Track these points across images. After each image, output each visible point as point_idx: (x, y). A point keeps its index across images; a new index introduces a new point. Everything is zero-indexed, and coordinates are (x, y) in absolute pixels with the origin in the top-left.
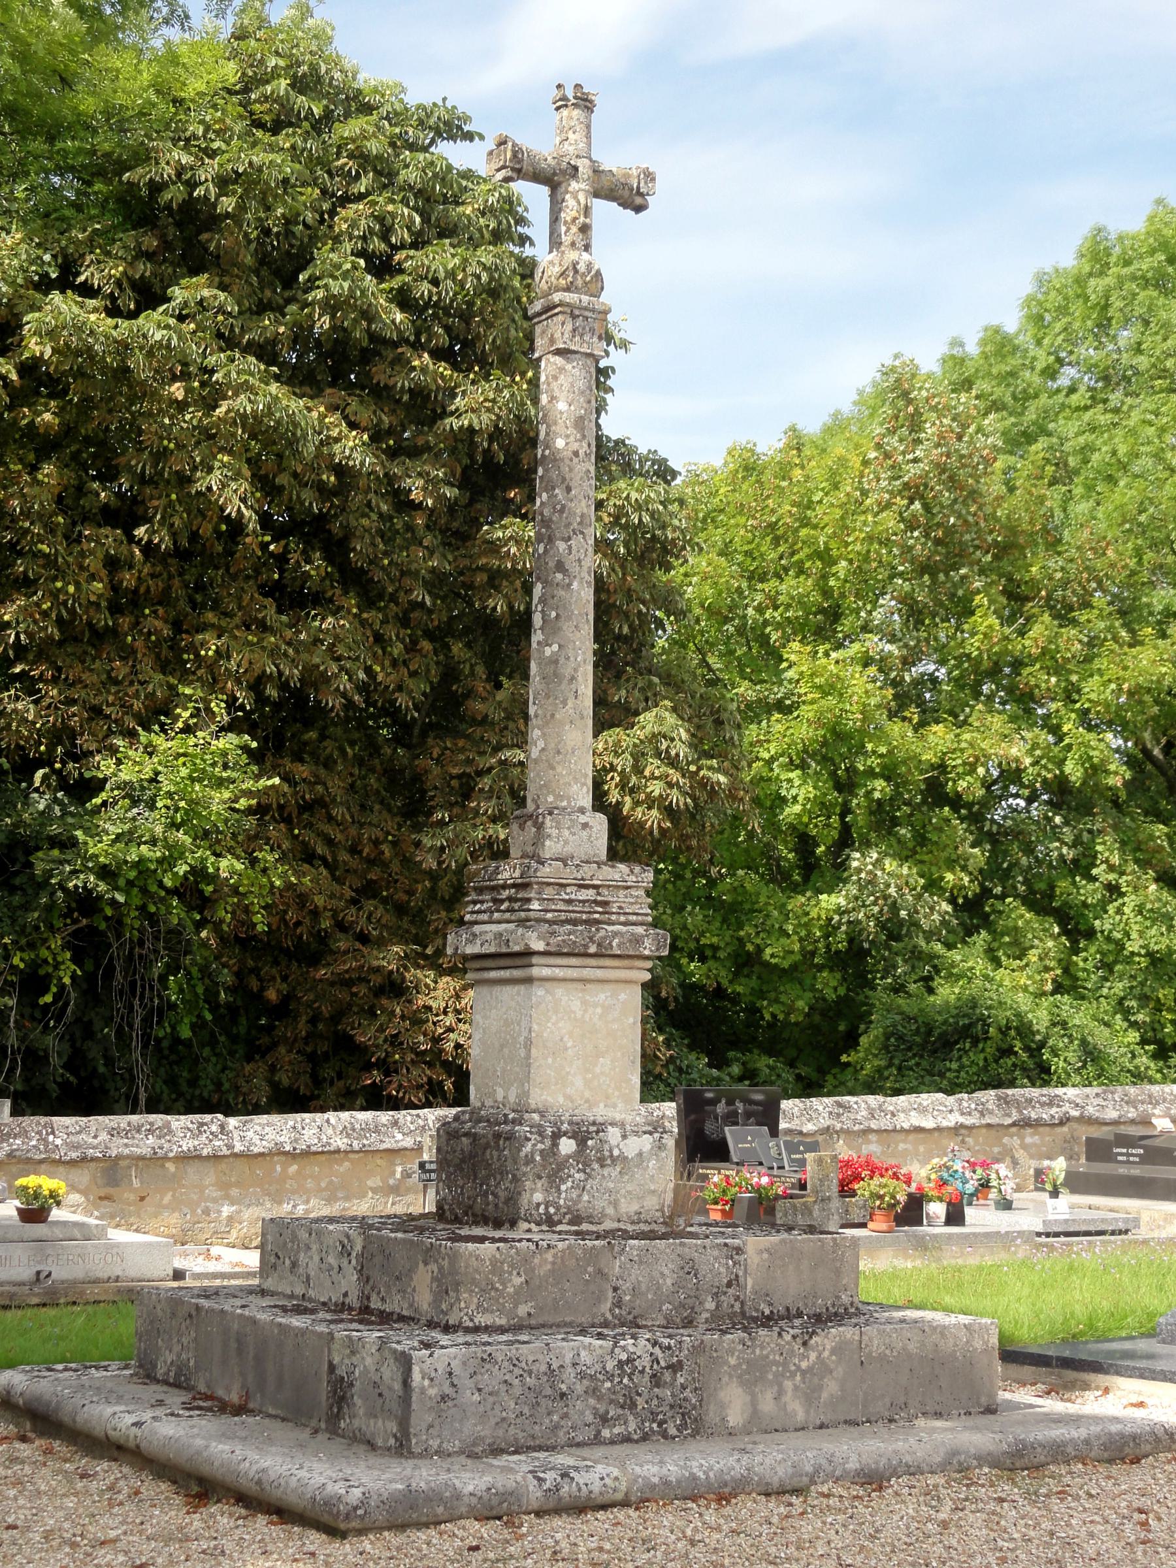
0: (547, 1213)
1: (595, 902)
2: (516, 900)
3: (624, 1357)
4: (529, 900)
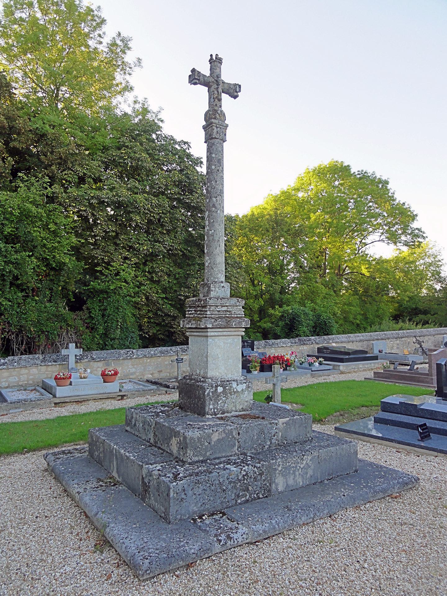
0: (214, 411)
1: (227, 311)
2: (202, 311)
3: (245, 473)
4: (206, 311)
